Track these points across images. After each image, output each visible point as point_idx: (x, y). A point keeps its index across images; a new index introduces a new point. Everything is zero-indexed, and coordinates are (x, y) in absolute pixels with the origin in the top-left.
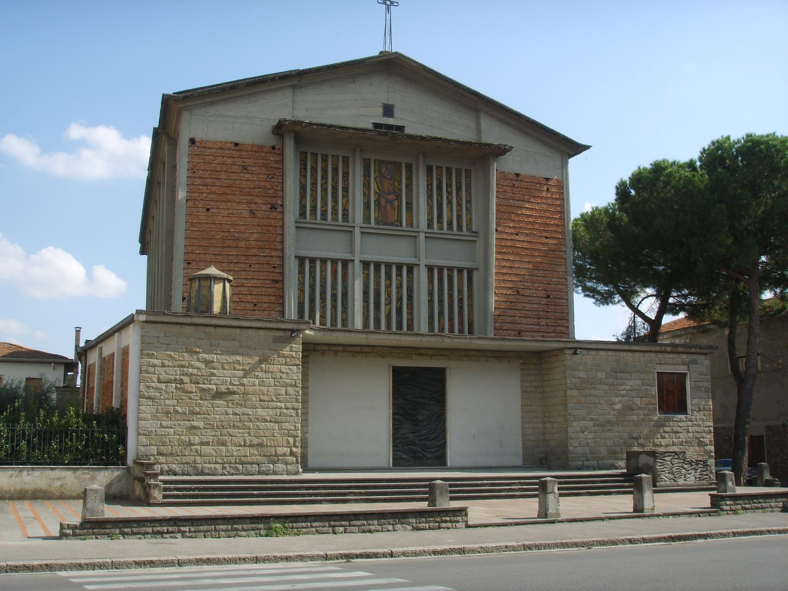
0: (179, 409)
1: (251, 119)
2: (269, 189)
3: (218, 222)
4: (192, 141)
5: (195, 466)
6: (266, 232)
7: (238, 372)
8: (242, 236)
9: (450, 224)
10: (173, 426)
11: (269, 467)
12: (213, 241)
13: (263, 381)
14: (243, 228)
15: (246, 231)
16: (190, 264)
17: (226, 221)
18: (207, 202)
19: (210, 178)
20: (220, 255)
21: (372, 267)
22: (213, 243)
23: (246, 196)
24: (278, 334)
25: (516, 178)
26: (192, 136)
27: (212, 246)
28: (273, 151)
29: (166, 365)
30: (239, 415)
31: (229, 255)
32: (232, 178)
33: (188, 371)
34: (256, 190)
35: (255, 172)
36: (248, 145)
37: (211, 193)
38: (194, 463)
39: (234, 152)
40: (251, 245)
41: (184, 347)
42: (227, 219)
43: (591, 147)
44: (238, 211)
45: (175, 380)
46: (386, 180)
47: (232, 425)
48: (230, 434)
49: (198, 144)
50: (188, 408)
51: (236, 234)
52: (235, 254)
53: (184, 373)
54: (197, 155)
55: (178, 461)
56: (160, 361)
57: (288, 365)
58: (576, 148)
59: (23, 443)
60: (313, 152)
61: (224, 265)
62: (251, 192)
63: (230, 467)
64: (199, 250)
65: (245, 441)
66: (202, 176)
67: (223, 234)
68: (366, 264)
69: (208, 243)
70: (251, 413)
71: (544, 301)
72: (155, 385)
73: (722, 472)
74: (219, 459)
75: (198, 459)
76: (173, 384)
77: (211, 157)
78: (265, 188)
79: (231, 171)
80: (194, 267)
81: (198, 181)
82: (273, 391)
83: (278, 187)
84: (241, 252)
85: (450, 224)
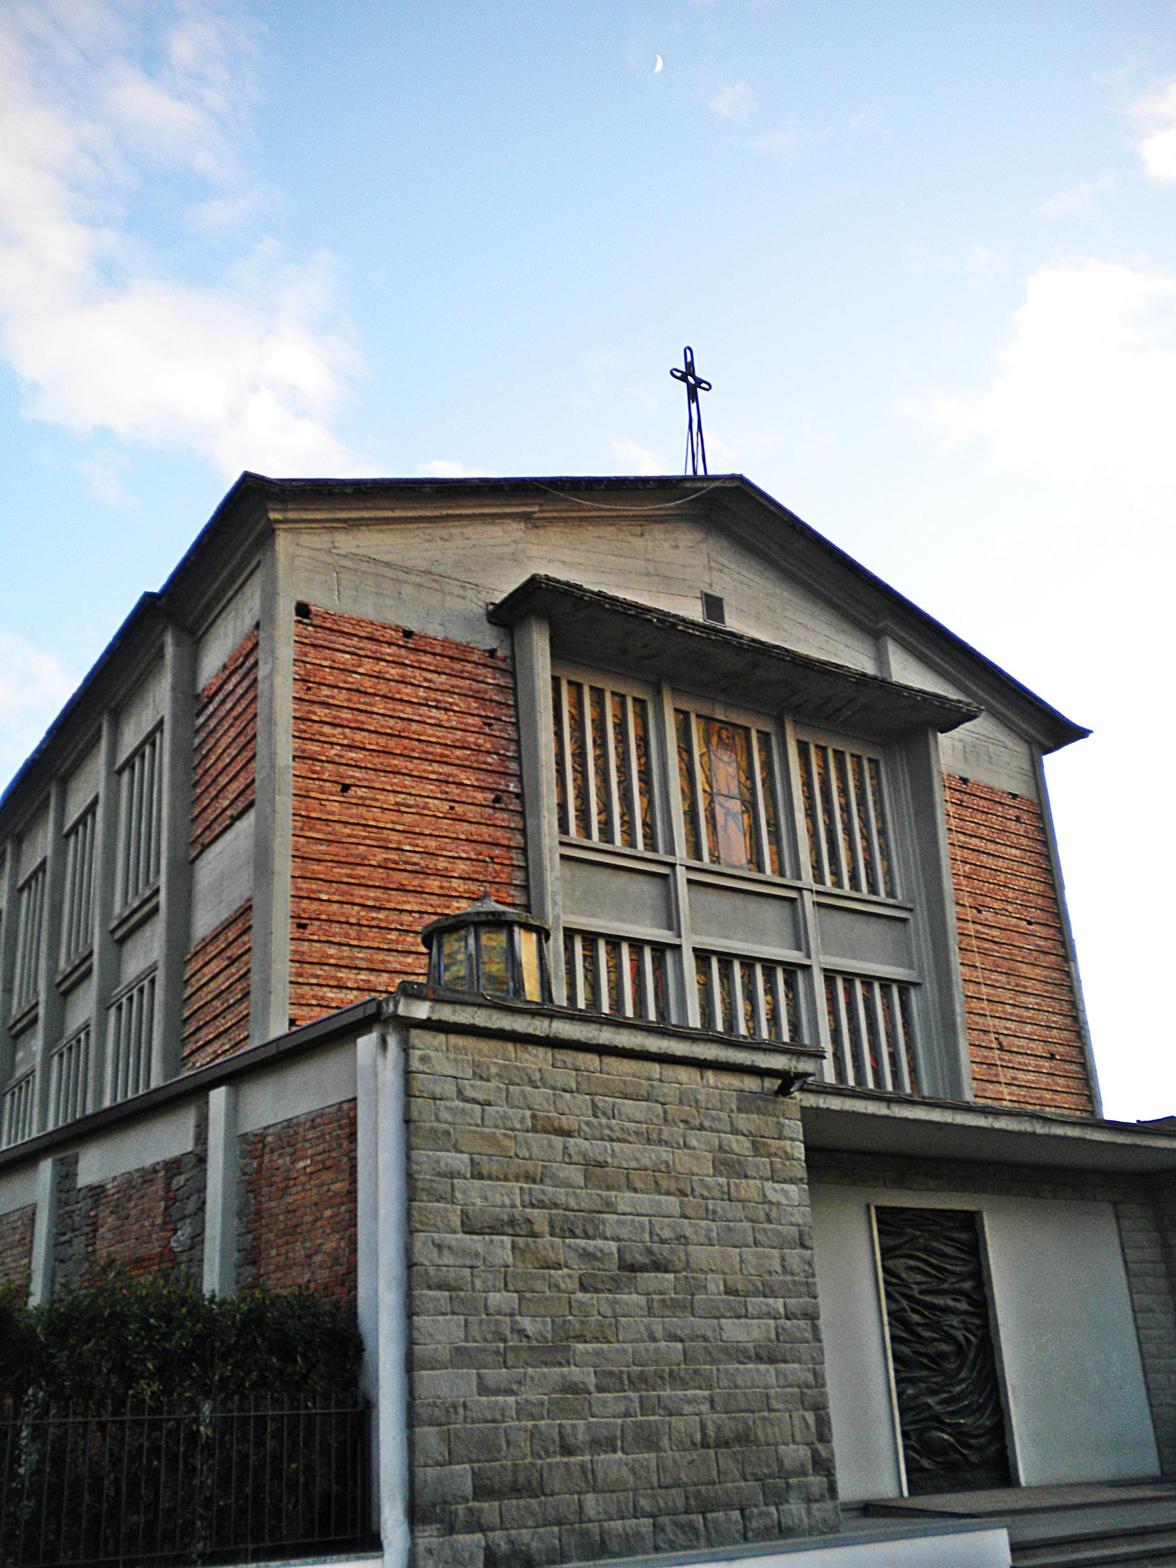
0: (526, 1323)
1: (437, 578)
2: (488, 753)
3: (374, 823)
4: (303, 610)
5: (581, 1529)
6: (488, 859)
7: (666, 1197)
8: (431, 863)
9: (854, 877)
10: (514, 1387)
11: (769, 1514)
12: (360, 871)
13: (730, 1229)
14: (432, 844)
15: (440, 852)
16: (304, 926)
17: (393, 822)
18: (342, 769)
19: (348, 708)
20: (380, 908)
21: (737, 966)
22: (364, 877)
23: (435, 765)
24: (751, 1083)
27: (360, 885)
28: (490, 662)
29: (485, 1172)
30: (682, 1341)
31: (402, 911)
32: (402, 715)
33: (544, 1192)
34: (458, 752)
35: (455, 708)
36: (435, 639)
37: (350, 747)
38: (581, 1521)
39: (403, 651)
40: (456, 890)
41: (528, 1113)
42: (394, 816)
43: (1083, 733)
44: (418, 799)
45: (512, 1222)
46: (721, 764)
47: (666, 1376)
48: (665, 1408)
49: (316, 621)
50: (549, 1320)
51: (416, 858)
52: (416, 908)
53: (535, 1202)
54: (314, 646)
55: (533, 1515)
57: (778, 1182)
58: (1059, 731)
60: (573, 678)
61: (389, 937)
62: (447, 756)
63: (676, 1524)
64: (327, 893)
65: (703, 1427)
66: (331, 701)
67: (385, 856)
68: (703, 956)
69: (349, 876)
70: (709, 1334)
72: (457, 1239)
74: (645, 1497)
75: (591, 1501)
76: (505, 1238)
77: (348, 656)
78: (479, 751)
79: (398, 696)
80: (315, 938)
81: (321, 713)
82: (754, 1262)
83: (507, 750)
84: (431, 905)
85: (854, 877)
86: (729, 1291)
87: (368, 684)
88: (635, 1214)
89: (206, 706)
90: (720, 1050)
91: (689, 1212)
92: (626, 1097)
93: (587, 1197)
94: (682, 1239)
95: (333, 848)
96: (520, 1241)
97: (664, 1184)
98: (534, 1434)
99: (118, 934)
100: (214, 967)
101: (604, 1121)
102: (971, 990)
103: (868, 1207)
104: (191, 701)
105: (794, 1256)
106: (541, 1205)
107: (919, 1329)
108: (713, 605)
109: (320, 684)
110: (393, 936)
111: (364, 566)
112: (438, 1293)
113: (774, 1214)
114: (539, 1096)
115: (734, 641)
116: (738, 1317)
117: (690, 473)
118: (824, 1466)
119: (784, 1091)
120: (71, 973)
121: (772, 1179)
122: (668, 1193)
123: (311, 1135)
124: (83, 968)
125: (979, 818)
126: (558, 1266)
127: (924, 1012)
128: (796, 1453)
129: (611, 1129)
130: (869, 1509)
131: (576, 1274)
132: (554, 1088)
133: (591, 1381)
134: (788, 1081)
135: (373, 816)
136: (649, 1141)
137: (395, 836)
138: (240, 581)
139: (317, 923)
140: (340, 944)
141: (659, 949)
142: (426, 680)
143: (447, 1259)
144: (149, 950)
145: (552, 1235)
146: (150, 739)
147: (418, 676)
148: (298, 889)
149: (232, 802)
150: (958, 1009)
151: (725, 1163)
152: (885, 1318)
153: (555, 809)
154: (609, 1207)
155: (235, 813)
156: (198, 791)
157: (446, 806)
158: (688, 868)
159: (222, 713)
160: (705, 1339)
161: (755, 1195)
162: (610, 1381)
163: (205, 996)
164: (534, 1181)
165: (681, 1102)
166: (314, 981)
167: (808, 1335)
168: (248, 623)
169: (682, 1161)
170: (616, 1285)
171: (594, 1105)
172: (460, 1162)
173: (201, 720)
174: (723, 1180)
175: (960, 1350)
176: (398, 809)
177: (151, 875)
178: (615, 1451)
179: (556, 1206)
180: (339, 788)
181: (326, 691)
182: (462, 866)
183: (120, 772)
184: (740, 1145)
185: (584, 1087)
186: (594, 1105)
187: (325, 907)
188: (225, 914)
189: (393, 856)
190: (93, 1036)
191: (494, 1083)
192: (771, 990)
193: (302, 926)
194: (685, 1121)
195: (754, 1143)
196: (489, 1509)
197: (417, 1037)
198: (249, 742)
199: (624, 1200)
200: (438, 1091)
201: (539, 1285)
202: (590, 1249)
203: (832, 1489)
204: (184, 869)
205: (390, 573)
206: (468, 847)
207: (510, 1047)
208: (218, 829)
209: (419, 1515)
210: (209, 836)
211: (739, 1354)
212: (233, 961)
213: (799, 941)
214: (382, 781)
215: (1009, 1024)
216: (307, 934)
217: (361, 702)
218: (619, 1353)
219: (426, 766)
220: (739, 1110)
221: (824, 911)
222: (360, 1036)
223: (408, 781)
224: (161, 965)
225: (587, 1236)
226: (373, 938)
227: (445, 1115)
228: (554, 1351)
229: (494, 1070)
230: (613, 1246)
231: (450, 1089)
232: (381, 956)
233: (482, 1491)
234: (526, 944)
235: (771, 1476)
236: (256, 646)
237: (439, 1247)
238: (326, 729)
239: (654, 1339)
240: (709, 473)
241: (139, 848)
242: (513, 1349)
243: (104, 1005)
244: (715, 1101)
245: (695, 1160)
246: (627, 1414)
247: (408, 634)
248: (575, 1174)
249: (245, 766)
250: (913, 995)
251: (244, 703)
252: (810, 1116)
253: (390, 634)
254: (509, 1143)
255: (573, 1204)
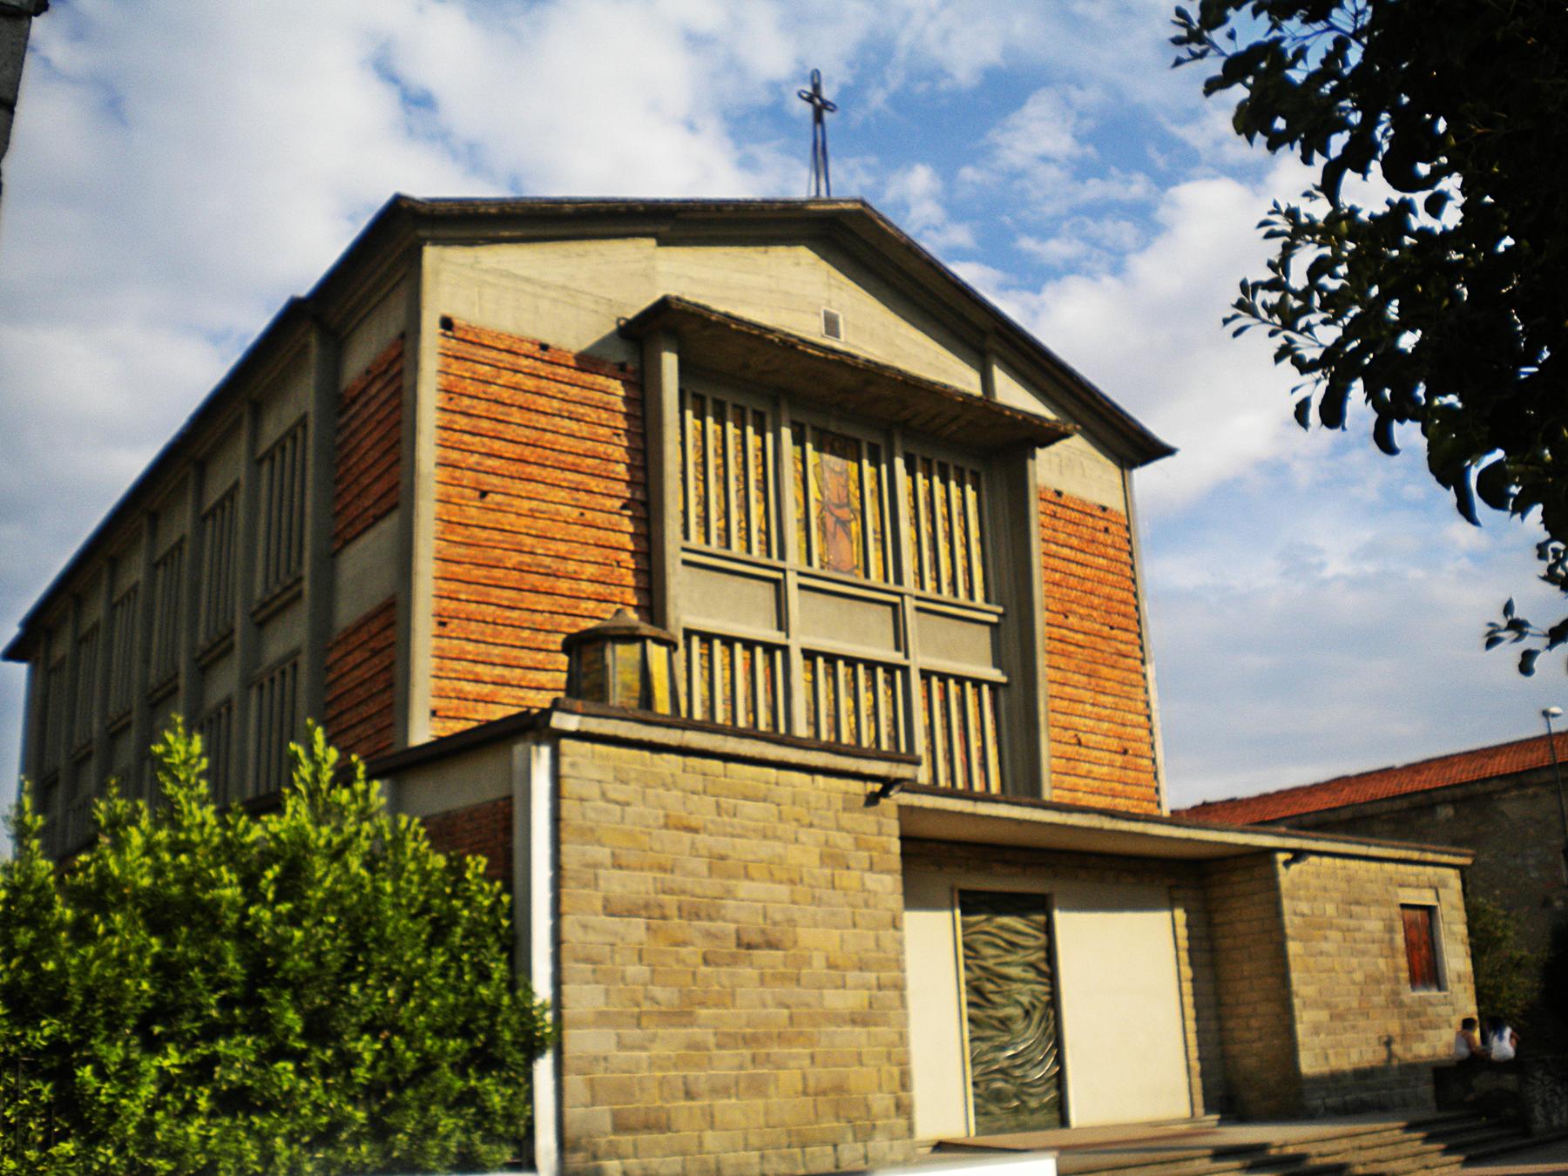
0: (657, 991)
4: (447, 323)
12: (498, 573)
13: (834, 914)
24: (856, 787)
25: (1055, 499)
26: (448, 312)
30: (788, 1007)
37: (489, 455)
41: (661, 812)
43: (1168, 451)
45: (647, 906)
49: (459, 334)
51: (548, 561)
54: (457, 358)
56: (607, 851)
59: (1015, 1103)
60: (698, 391)
65: (804, 1078)
71: (1119, 759)
73: (1448, 1115)
75: (710, 1138)
81: (462, 422)
86: (830, 966)
87: (506, 395)
88: (752, 900)
89: (348, 407)
90: (831, 755)
91: (798, 898)
92: (746, 798)
93: (712, 886)
94: (792, 922)
95: (473, 551)
96: (655, 923)
97: (778, 874)
98: (662, 1082)
99: (260, 617)
100: (358, 656)
101: (726, 819)
102: (1055, 689)
103: (952, 890)
104: (337, 402)
105: (888, 935)
106: (671, 892)
107: (991, 996)
108: (831, 325)
109: (461, 394)
110: (526, 633)
111: (504, 282)
112: (582, 966)
113: (872, 902)
114: (672, 797)
115: (849, 361)
116: (837, 988)
117: (813, 194)
118: (903, 1109)
119: (884, 793)
120: (210, 650)
121: (871, 869)
122: (781, 882)
123: (469, 826)
124: (224, 645)
125: (1070, 528)
126: (684, 944)
127: (1008, 709)
128: (882, 1102)
129: (732, 826)
130: (941, 1147)
131: (701, 951)
132: (684, 790)
133: (712, 1041)
134: (888, 784)
135: (508, 520)
136: (765, 837)
137: (528, 541)
138: (385, 290)
139: (456, 621)
140: (477, 641)
141: (770, 649)
142: (561, 392)
143: (592, 937)
144: (291, 634)
145: (680, 917)
146: (291, 434)
147: (553, 388)
148: (439, 589)
149: (375, 503)
150: (1042, 707)
151: (832, 856)
152: (963, 986)
153: (680, 515)
154: (729, 893)
155: (379, 512)
156: (340, 487)
157: (575, 513)
158: (800, 574)
159: (365, 415)
160: (808, 1005)
161: (855, 884)
162: (727, 1040)
163: (348, 682)
164: (665, 871)
165: (794, 803)
166: (453, 675)
167: (897, 1003)
168: (393, 331)
169: (794, 855)
170: (734, 960)
171: (718, 805)
172: (603, 854)
173: (343, 420)
174: (828, 871)
175: (1027, 1014)
176: (532, 514)
177: (293, 564)
178: (729, 1097)
179: (683, 892)
180: (477, 494)
181: (466, 401)
182: (590, 570)
183: (260, 462)
184: (843, 841)
185: (710, 790)
186: (718, 805)
187: (463, 606)
188: (367, 608)
189: (527, 559)
190: (236, 713)
191: (633, 786)
192: (874, 688)
193: (443, 624)
194: (797, 820)
195: (856, 839)
196: (626, 1140)
197: (566, 744)
198: (393, 446)
199: (743, 888)
200: (584, 793)
201: (670, 960)
202: (713, 930)
203: (911, 1129)
204: (328, 561)
205: (529, 288)
206: (597, 551)
207: (646, 754)
208: (359, 526)
209: (568, 1145)
210: (350, 532)
211: (836, 1018)
212: (376, 653)
213: (900, 643)
214: (518, 487)
215: (1088, 722)
216: (446, 631)
217: (498, 411)
218: (735, 1017)
219: (558, 474)
220: (845, 809)
221: (922, 615)
222: (515, 743)
223: (541, 488)
224: (305, 650)
225: (710, 918)
226: (508, 635)
227: (591, 814)
228: (680, 1016)
229: (633, 775)
230: (732, 927)
231: (594, 791)
232: (516, 652)
233: (620, 1127)
234: (657, 654)
235: (860, 1118)
236: (400, 355)
237: (585, 927)
238: (467, 438)
239: (764, 1006)
240: (834, 195)
241: (279, 537)
242: (648, 1013)
243: (247, 683)
244: (823, 803)
245: (804, 855)
246: (741, 1067)
247: (544, 347)
248: (701, 865)
249: (388, 469)
250: (1002, 693)
251: (388, 409)
252: (905, 811)
253: (527, 348)
254: (645, 838)
255: (698, 891)
